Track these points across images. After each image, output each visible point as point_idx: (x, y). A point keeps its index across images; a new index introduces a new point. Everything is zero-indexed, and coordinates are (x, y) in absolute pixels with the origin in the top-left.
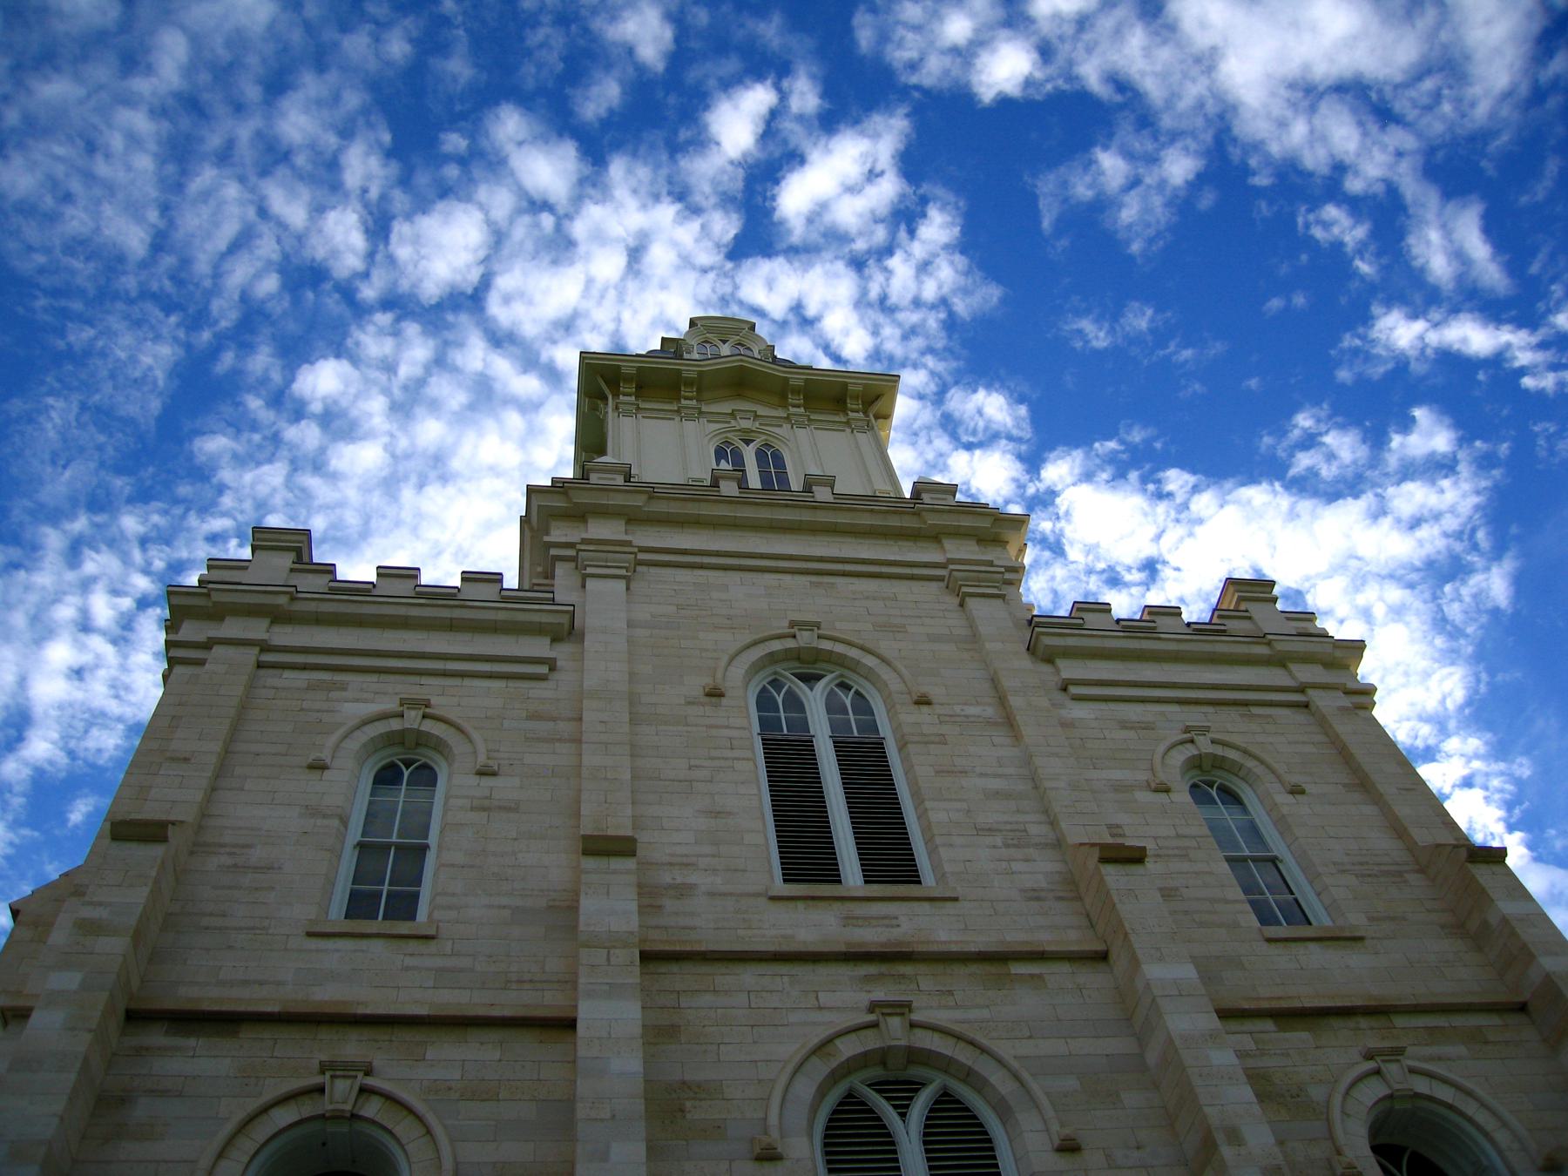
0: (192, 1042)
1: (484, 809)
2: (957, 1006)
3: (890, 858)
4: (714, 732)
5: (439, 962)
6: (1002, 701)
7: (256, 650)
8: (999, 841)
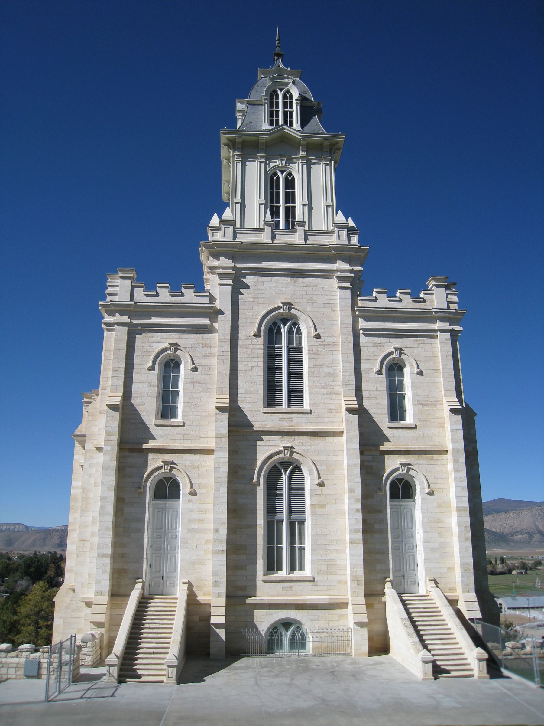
0: (134, 454)
1: (192, 382)
2: (302, 446)
3: (295, 398)
4: (254, 351)
5: (184, 432)
6: (425, 421)
7: (130, 281)
8: (325, 392)
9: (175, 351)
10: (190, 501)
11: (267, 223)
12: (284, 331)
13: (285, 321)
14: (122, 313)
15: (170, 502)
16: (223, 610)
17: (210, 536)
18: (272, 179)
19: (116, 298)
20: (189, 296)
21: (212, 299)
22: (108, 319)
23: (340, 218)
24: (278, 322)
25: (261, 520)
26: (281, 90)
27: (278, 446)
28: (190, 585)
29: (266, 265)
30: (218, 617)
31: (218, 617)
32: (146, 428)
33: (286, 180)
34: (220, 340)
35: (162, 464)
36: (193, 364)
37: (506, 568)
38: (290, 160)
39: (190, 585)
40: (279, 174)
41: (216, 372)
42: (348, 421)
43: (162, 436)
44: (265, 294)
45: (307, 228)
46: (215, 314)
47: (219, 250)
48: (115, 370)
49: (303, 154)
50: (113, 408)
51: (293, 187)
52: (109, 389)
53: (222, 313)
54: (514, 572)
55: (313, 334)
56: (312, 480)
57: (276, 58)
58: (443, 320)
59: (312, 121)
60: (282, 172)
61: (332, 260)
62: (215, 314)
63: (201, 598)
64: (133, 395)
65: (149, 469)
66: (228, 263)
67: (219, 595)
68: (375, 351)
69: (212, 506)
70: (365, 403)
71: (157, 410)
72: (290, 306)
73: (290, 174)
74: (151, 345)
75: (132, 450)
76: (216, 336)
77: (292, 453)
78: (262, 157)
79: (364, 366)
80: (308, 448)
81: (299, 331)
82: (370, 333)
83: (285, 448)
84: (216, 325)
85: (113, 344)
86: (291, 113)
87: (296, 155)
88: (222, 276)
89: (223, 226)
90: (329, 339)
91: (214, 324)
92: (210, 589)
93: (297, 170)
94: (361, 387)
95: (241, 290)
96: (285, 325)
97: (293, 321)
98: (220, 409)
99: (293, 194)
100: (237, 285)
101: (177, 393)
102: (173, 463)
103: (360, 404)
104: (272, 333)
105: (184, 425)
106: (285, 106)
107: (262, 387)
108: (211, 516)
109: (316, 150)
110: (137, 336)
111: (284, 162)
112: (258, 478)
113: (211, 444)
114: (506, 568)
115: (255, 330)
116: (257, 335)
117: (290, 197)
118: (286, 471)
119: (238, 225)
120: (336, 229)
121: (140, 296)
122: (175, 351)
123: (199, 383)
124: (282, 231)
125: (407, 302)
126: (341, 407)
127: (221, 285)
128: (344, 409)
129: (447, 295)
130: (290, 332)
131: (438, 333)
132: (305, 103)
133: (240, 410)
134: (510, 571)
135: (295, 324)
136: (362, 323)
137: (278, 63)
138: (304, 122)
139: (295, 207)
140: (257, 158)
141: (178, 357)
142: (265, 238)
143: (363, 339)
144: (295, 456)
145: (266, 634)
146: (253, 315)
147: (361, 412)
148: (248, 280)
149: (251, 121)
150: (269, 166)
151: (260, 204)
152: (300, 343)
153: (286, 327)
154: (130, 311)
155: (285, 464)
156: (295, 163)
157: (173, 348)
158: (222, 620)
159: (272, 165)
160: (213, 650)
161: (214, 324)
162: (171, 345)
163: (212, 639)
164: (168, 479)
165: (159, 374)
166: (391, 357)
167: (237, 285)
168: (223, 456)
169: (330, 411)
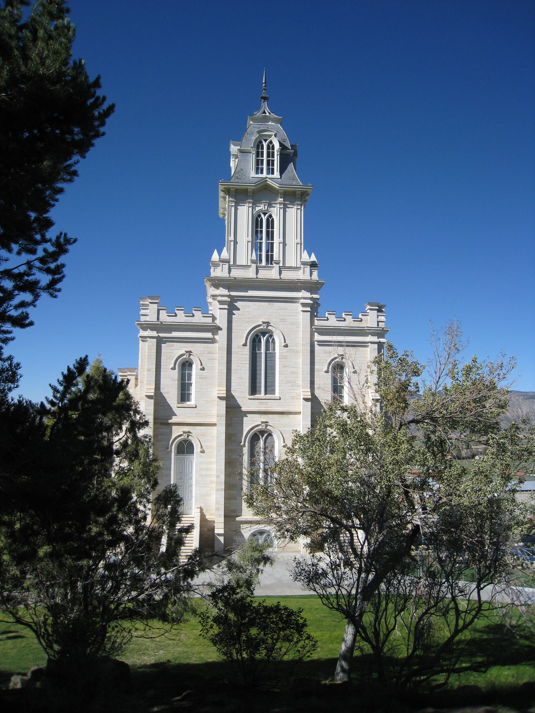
0: (164, 426)
3: (270, 388)
4: (242, 356)
9: (189, 356)
10: (201, 457)
11: (253, 262)
12: (263, 340)
13: (264, 333)
14: (152, 329)
15: (187, 457)
16: (222, 525)
17: (214, 479)
18: (257, 220)
19: (147, 318)
20: (198, 318)
21: (214, 318)
22: (142, 333)
23: (305, 257)
24: (259, 334)
25: (246, 458)
26: (266, 140)
27: (258, 421)
28: (201, 509)
29: (251, 293)
30: (219, 530)
31: (219, 530)
32: (171, 408)
33: (268, 220)
34: (220, 349)
35: (182, 433)
36: (202, 365)
37: (470, 453)
38: (270, 205)
39: (201, 509)
40: (262, 216)
41: (217, 371)
42: (304, 406)
43: (181, 414)
44: (251, 315)
45: (281, 265)
46: (216, 329)
47: (218, 283)
48: (149, 370)
49: (281, 200)
50: (149, 397)
51: (273, 227)
52: (145, 382)
53: (221, 329)
54: (477, 458)
55: (283, 344)
56: (279, 443)
57: (263, 100)
58: (373, 334)
59: (289, 167)
60: (265, 214)
61: (298, 290)
62: (216, 329)
63: (208, 517)
64: (161, 387)
65: (173, 437)
66: (225, 292)
67: (220, 516)
68: (325, 356)
69: (215, 460)
70: (317, 393)
71: (178, 397)
72: (268, 324)
73: (270, 216)
74: (172, 352)
75: (162, 424)
76: (216, 345)
77: (267, 426)
78: (249, 203)
79: (316, 367)
80: (278, 422)
81: (273, 341)
82: (322, 343)
83: (262, 422)
84: (217, 337)
85: (147, 350)
86: (273, 161)
87: (276, 201)
88: (221, 302)
89: (221, 264)
90: (294, 348)
91: (216, 337)
92: (214, 512)
93: (276, 212)
94: (314, 381)
95: (234, 311)
96: (264, 337)
97: (270, 334)
98: (221, 398)
99: (273, 232)
100: (231, 307)
101: (191, 384)
102: (189, 432)
103: (313, 394)
104: (255, 342)
105: (196, 407)
106: (268, 156)
107: (248, 381)
108: (214, 466)
109: (291, 196)
110: (162, 345)
111: (266, 207)
112: (245, 442)
113: (214, 420)
114: (470, 453)
115: (244, 342)
116: (245, 345)
117: (270, 235)
118: (262, 437)
119: (232, 263)
120: (302, 266)
121: (164, 317)
122: (189, 356)
123: (205, 378)
124: (264, 267)
125: (349, 322)
126: (300, 395)
127: (220, 309)
128: (302, 398)
129: (378, 316)
130: (267, 342)
131: (369, 344)
132: (284, 152)
133: (233, 397)
134: (473, 456)
135: (271, 336)
136: (317, 337)
137: (263, 107)
138: (282, 170)
139: (273, 243)
140: (246, 203)
141: (191, 360)
142: (250, 274)
143: (317, 348)
144: (268, 427)
145: (248, 539)
146: (242, 330)
147: (313, 400)
148: (238, 304)
149: (242, 168)
150: (255, 210)
151: (248, 242)
152: (274, 350)
153: (265, 338)
154: (157, 327)
155: (262, 432)
156: (275, 207)
157: (188, 354)
158: (222, 531)
159: (257, 209)
160: (217, 549)
161: (216, 337)
162: (187, 352)
163: (215, 542)
164: (185, 441)
165: (179, 372)
166: (336, 360)
167: (231, 307)
168: (222, 428)
169: (293, 398)
